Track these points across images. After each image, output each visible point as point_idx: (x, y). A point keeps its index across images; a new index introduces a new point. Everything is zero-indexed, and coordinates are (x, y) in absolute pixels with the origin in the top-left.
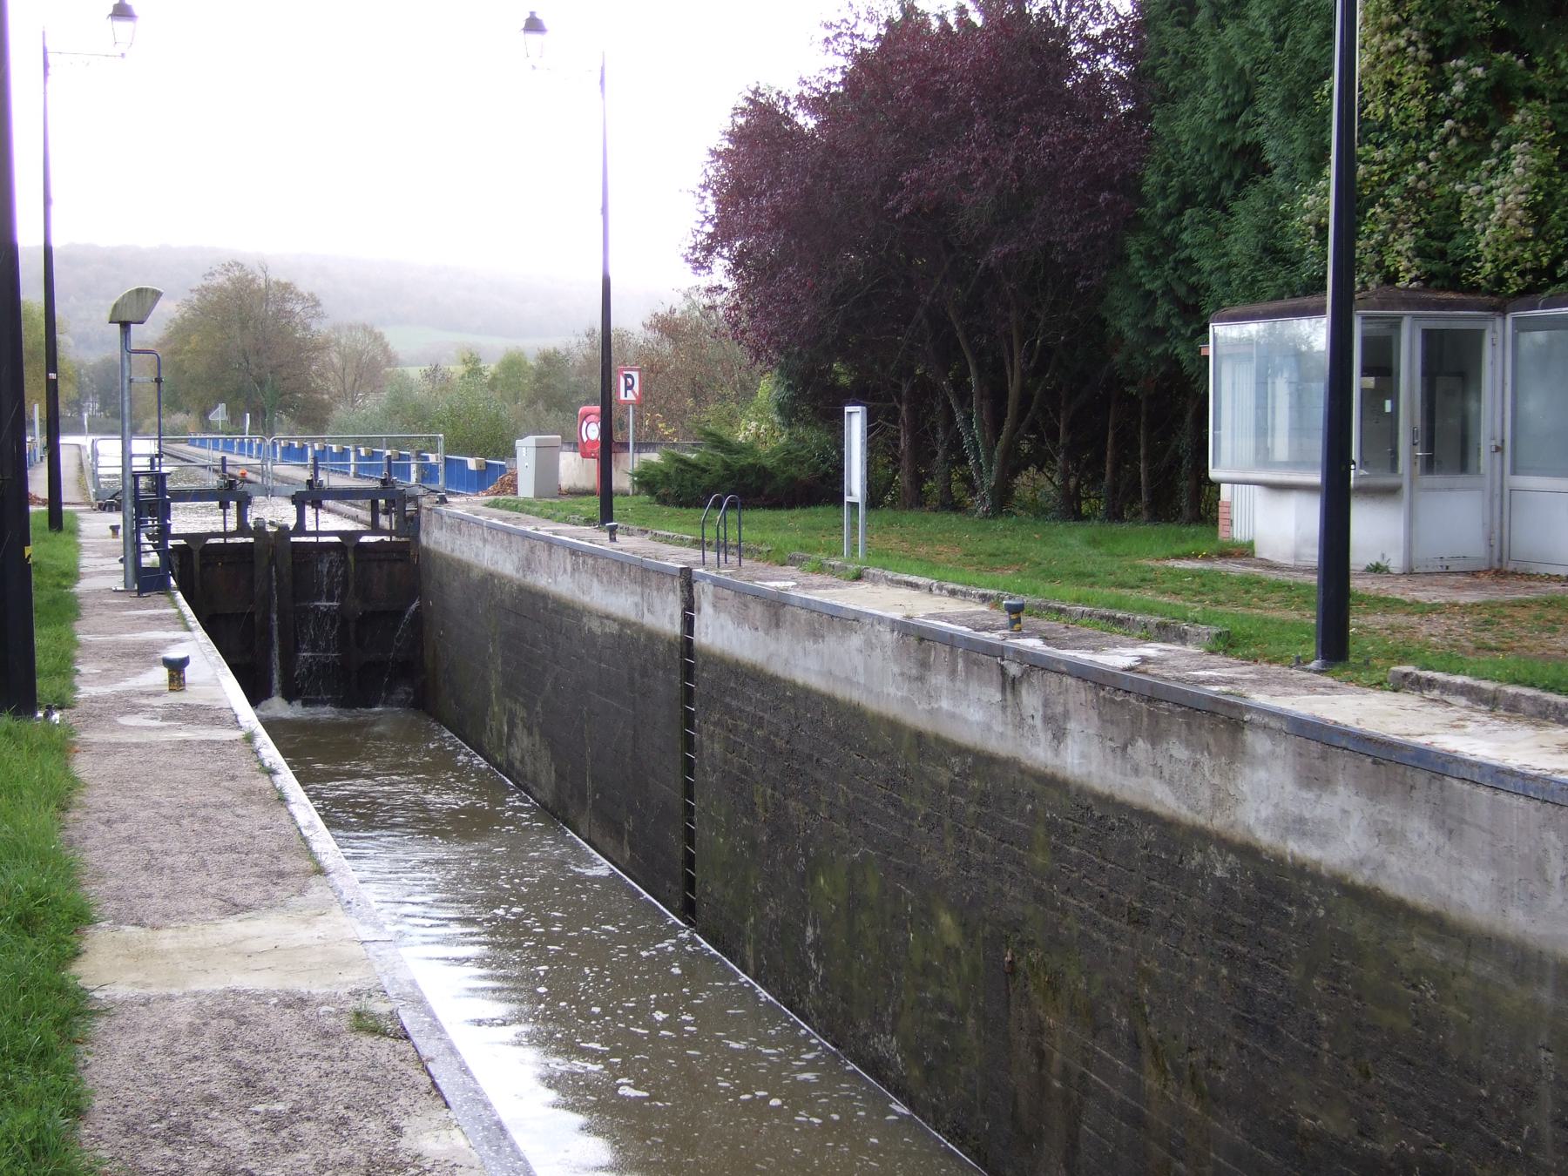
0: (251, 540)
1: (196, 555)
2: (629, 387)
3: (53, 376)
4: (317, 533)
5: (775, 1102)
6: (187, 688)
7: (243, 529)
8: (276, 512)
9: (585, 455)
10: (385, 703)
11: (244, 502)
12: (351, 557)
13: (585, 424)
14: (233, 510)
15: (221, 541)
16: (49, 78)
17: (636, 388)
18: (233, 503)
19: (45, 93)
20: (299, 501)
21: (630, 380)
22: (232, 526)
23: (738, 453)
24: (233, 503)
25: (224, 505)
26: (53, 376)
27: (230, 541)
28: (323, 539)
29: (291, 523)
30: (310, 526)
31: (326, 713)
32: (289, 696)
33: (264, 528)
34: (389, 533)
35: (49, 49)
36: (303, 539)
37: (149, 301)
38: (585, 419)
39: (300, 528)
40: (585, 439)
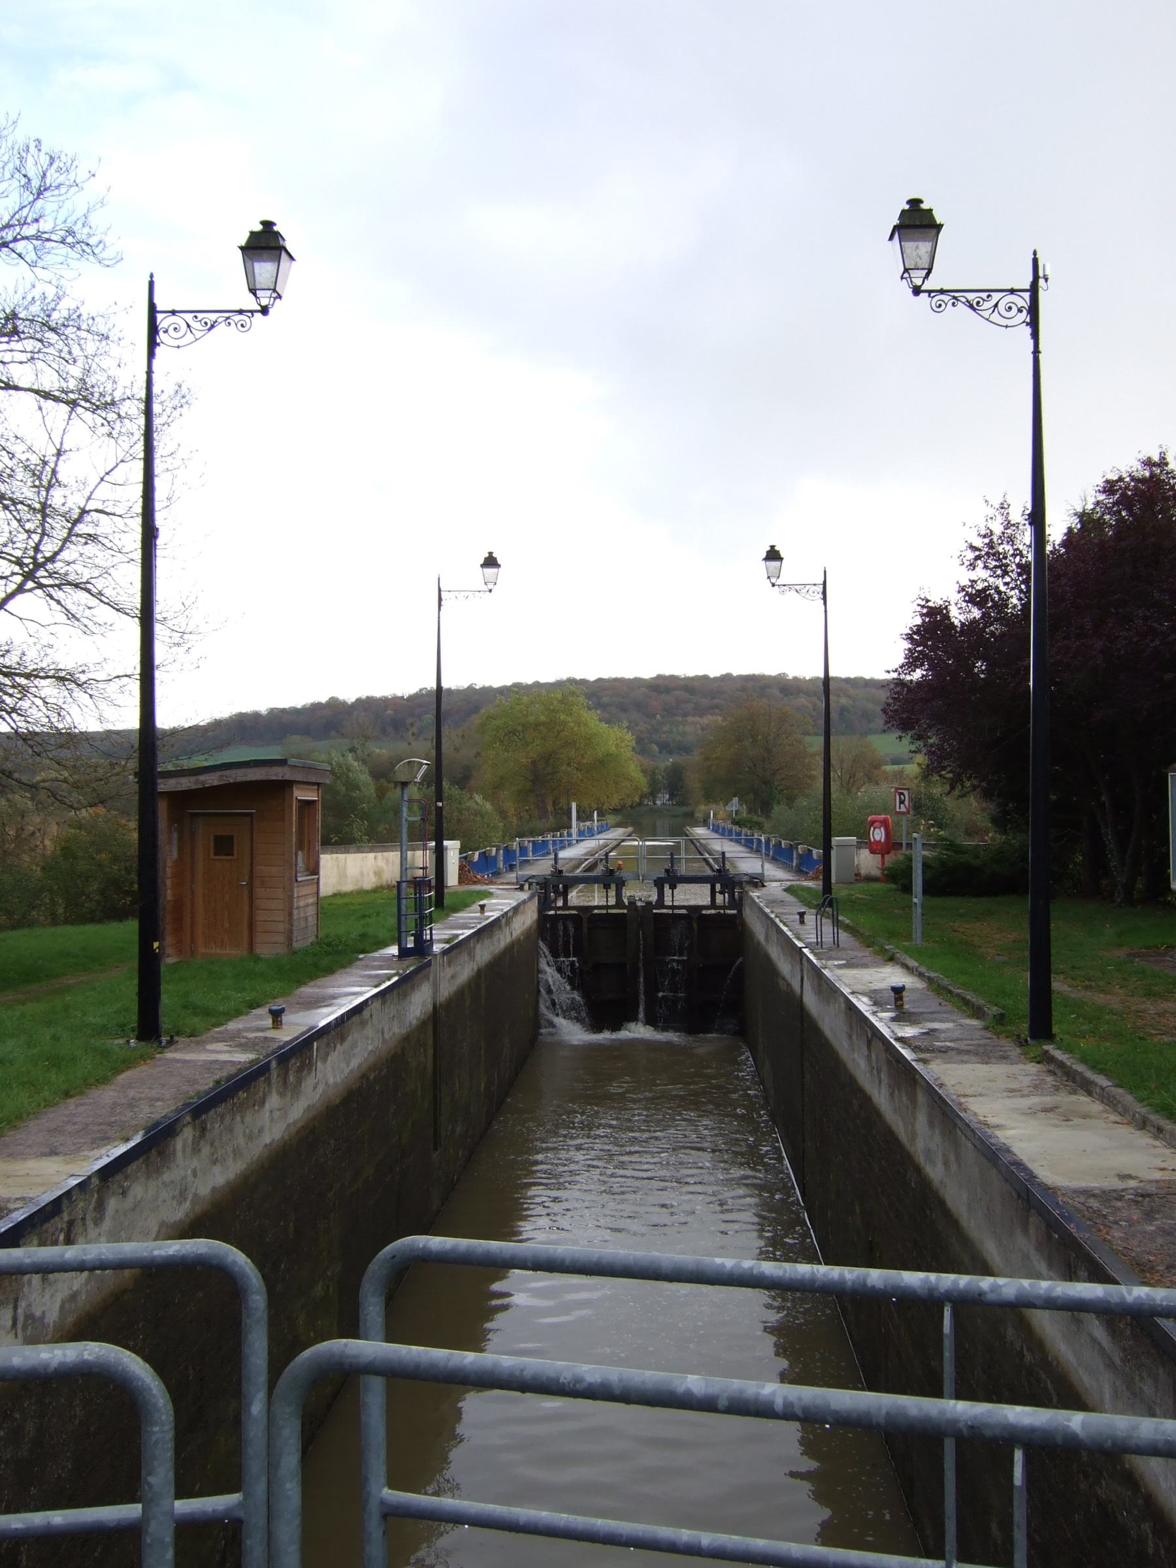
0: (625, 911)
1: (585, 921)
2: (902, 802)
3: (440, 804)
4: (673, 907)
5: (668, 1341)
6: (284, 1026)
7: (619, 903)
8: (640, 892)
9: (872, 852)
10: (717, 1031)
11: (620, 884)
12: (695, 925)
13: (872, 828)
14: (612, 893)
15: (604, 912)
16: (442, 608)
17: (907, 803)
18: (613, 886)
19: (439, 618)
20: (659, 884)
21: (902, 796)
22: (612, 901)
23: (965, 853)
24: (613, 886)
25: (607, 887)
26: (440, 804)
27: (610, 911)
28: (677, 911)
29: (654, 898)
30: (668, 902)
31: (672, 1036)
32: (651, 1021)
33: (634, 903)
34: (723, 907)
35: (442, 589)
36: (664, 911)
37: (416, 769)
38: (872, 825)
39: (660, 903)
40: (872, 840)
